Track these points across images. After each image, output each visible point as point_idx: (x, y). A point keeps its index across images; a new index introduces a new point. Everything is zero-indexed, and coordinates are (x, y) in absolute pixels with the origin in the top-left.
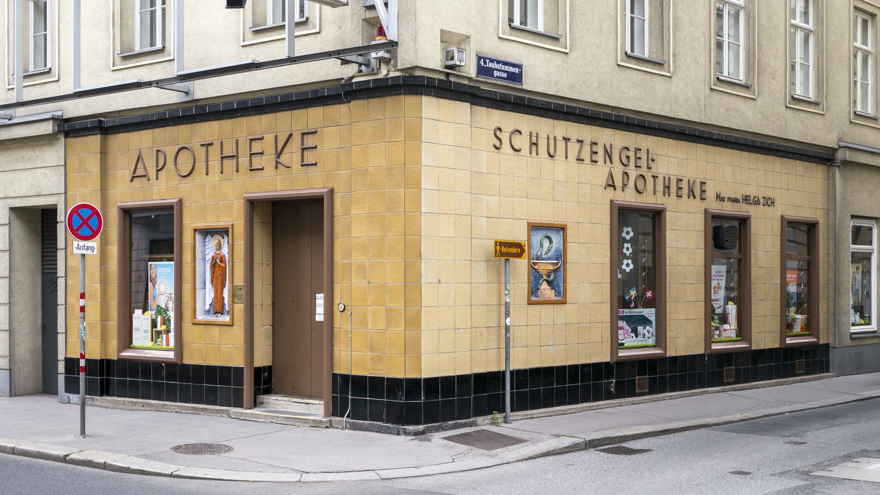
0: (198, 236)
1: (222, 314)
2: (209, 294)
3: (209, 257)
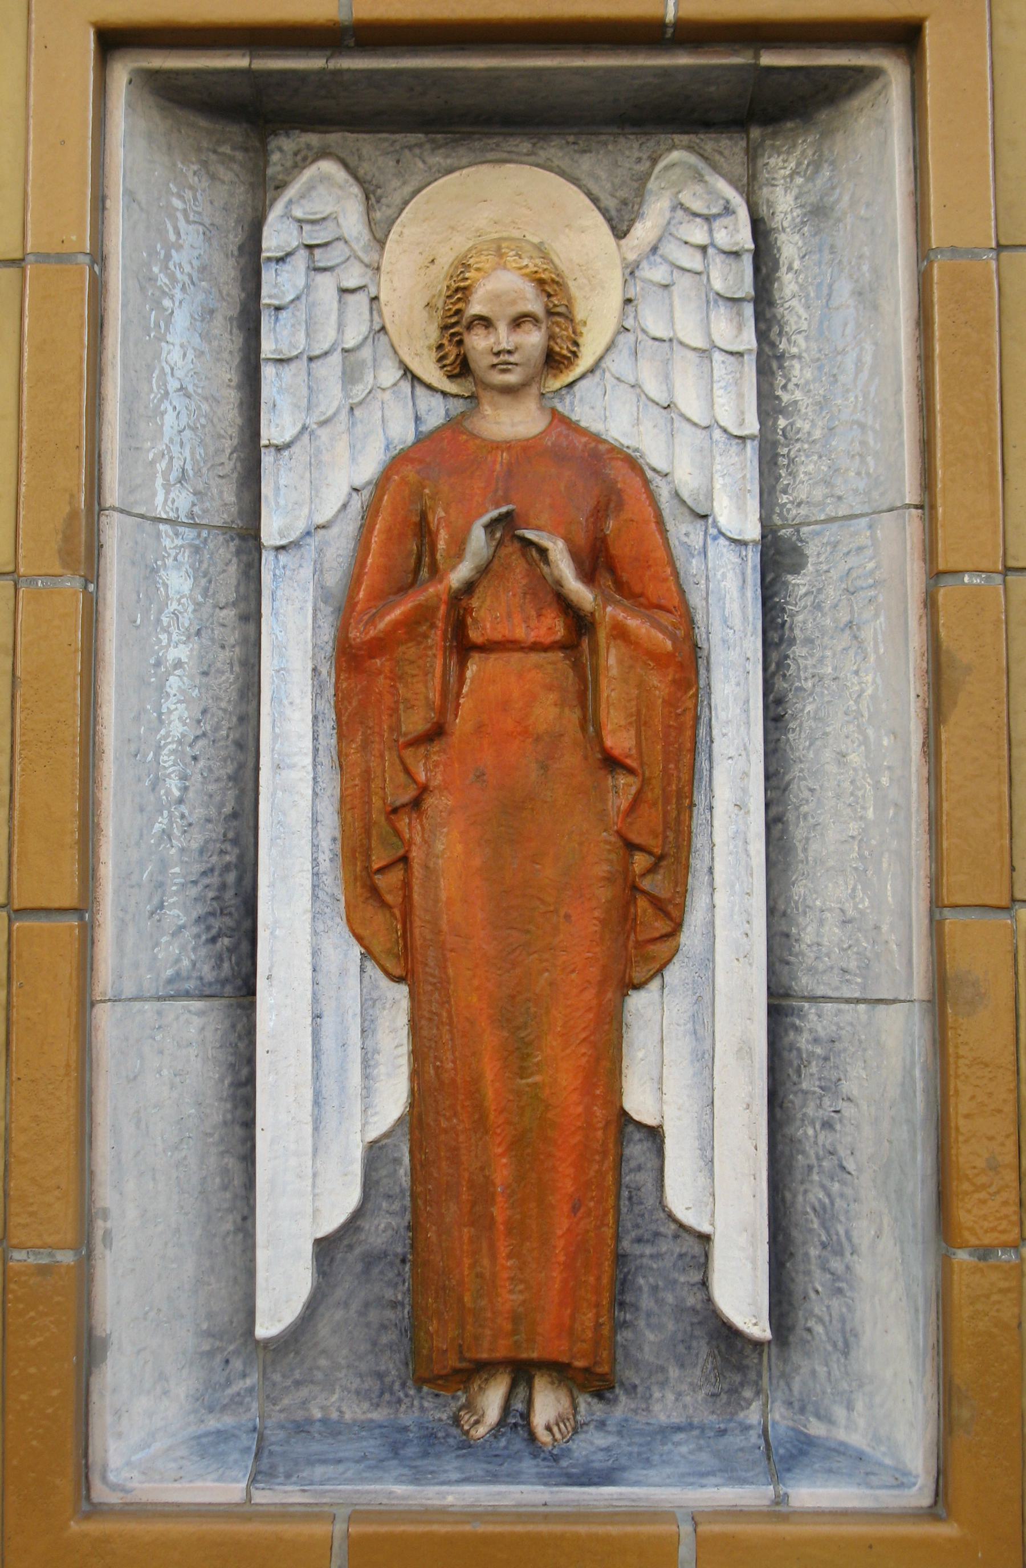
0: (159, 208)
1: (593, 1380)
3: (323, 485)
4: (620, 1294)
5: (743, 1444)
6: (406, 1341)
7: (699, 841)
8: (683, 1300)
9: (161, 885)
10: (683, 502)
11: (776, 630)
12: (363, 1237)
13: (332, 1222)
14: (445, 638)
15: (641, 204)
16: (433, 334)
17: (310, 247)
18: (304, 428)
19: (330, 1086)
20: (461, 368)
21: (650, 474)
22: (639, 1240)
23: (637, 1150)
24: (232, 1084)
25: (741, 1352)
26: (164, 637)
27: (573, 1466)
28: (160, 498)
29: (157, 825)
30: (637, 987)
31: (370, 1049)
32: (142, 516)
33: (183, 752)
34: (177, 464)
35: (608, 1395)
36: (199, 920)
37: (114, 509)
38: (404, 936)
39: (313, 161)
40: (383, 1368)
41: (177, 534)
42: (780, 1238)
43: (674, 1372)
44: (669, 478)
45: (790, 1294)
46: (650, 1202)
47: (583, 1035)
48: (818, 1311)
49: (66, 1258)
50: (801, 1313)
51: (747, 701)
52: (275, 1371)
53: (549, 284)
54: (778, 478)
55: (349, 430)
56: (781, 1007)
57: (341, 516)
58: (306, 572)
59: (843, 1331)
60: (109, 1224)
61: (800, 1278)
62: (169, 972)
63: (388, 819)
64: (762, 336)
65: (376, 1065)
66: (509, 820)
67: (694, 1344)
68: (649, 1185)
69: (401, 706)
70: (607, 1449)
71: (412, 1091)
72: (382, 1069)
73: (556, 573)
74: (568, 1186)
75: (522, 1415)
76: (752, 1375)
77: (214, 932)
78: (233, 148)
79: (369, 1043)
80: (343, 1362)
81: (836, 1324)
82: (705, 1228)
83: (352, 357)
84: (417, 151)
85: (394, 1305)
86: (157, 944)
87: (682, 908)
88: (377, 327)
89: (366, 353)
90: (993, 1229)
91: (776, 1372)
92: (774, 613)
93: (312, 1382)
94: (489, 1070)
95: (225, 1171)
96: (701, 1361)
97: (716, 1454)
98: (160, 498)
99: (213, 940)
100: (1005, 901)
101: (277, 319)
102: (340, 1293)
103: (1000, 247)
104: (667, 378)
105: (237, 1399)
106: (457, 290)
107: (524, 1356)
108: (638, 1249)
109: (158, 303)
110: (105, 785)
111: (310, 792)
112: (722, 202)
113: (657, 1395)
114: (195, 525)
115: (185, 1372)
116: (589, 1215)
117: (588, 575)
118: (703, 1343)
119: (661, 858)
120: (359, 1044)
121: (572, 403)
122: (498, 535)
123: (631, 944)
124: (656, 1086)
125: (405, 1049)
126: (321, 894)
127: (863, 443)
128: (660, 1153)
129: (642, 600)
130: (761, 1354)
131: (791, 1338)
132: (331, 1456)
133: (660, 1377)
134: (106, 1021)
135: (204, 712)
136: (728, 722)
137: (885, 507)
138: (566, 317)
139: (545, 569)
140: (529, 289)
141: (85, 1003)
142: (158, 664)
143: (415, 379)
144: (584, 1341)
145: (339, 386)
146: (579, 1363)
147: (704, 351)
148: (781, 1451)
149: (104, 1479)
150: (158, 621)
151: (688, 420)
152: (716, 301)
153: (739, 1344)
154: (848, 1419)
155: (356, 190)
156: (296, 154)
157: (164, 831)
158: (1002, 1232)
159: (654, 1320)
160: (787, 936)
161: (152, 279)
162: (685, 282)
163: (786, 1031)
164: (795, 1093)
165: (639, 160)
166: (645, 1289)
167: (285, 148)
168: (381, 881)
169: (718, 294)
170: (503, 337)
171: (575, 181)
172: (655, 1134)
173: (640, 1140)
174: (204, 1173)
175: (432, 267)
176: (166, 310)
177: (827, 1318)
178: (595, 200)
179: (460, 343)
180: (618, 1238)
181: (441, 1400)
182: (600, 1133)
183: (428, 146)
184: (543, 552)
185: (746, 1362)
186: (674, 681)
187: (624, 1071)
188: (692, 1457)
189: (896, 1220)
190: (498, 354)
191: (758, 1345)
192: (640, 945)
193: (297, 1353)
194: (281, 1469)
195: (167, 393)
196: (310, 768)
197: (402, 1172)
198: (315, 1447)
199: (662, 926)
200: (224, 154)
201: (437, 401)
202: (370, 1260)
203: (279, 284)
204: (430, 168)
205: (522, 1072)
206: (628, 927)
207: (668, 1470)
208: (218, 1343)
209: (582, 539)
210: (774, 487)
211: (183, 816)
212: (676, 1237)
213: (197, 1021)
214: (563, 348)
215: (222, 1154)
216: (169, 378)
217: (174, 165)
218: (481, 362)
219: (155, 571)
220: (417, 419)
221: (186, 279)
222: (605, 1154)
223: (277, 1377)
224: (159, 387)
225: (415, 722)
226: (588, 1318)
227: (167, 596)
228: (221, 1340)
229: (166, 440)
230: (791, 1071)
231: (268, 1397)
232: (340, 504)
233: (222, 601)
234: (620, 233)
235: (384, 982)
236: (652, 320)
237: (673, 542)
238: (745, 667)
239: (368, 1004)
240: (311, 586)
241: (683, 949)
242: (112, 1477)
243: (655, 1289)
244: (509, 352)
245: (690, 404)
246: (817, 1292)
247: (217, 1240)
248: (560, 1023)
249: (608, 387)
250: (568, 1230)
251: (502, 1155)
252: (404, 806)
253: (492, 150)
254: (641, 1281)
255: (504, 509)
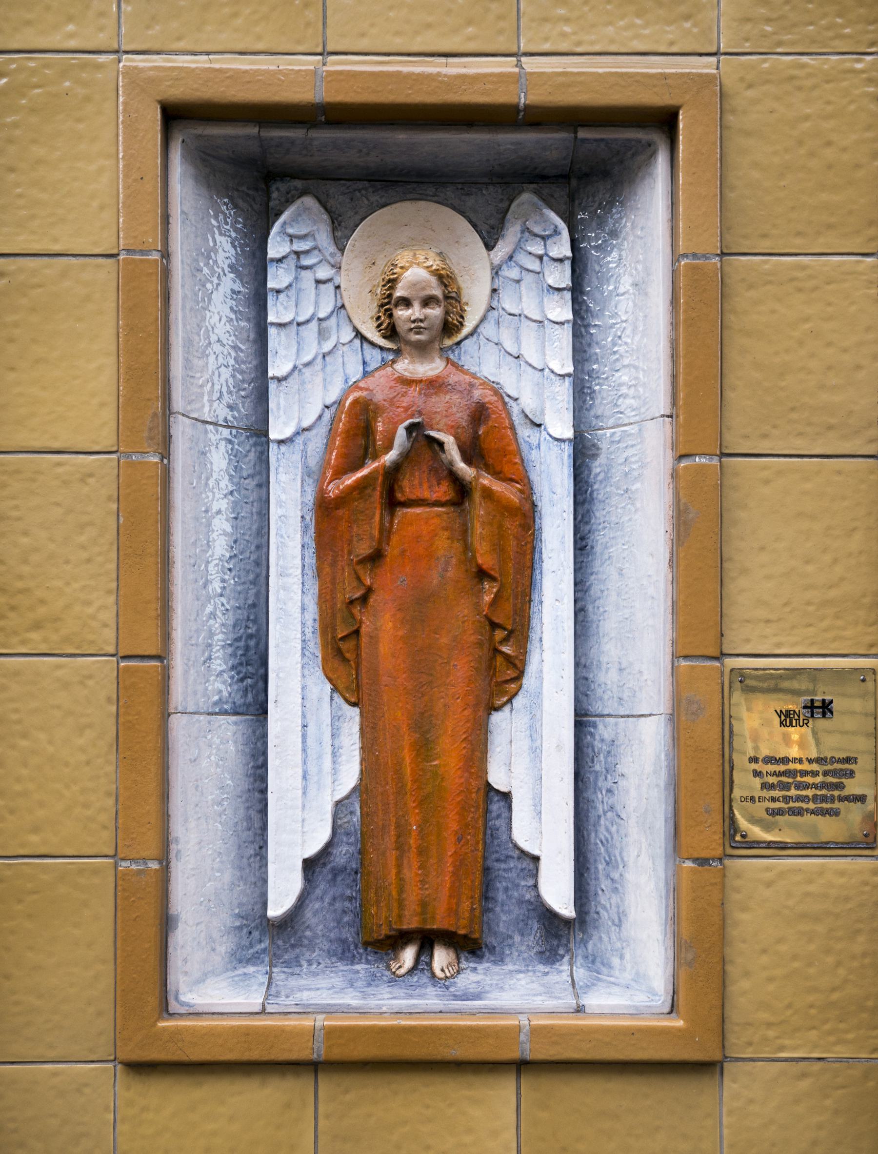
0: (202, 242)
2: (318, 761)
3: (300, 410)
4: (486, 895)
5: (559, 979)
6: (358, 920)
7: (535, 622)
8: (523, 896)
9: (210, 645)
10: (526, 416)
11: (582, 494)
12: (332, 859)
13: (313, 849)
14: (381, 497)
15: (502, 229)
16: (373, 309)
17: (298, 254)
18: (295, 367)
19: (312, 769)
20: (391, 332)
21: (507, 399)
22: (498, 860)
23: (496, 807)
24: (253, 767)
25: (557, 927)
26: (210, 494)
27: (457, 991)
28: (206, 409)
29: (207, 609)
30: (497, 709)
31: (336, 746)
32: (196, 419)
33: (223, 566)
34: (217, 387)
35: (478, 952)
36: (233, 668)
37: (179, 413)
38: (357, 678)
39: (299, 197)
40: (344, 937)
41: (217, 431)
42: (581, 859)
43: (517, 938)
44: (519, 402)
45: (587, 892)
46: (504, 837)
47: (464, 736)
48: (605, 901)
49: (154, 866)
50: (593, 903)
51: (564, 537)
52: (279, 938)
53: (444, 278)
54: (585, 401)
55: (323, 369)
56: (583, 722)
57: (318, 423)
58: (297, 457)
59: (618, 913)
60: (179, 847)
61: (593, 883)
62: (216, 698)
63: (347, 607)
64: (575, 312)
65: (340, 756)
66: (420, 609)
67: (530, 922)
68: (503, 828)
69: (355, 539)
70: (478, 982)
71: (361, 770)
72: (344, 758)
73: (449, 457)
74: (454, 826)
75: (426, 963)
76: (564, 941)
77: (241, 675)
78: (248, 188)
79: (336, 743)
80: (320, 933)
81: (615, 909)
82: (535, 852)
83: (324, 324)
84: (363, 192)
85: (351, 899)
86: (208, 681)
87: (524, 663)
88: (339, 305)
89: (333, 321)
90: (707, 848)
91: (578, 939)
92: (581, 484)
93: (301, 945)
94: (407, 757)
95: (249, 819)
96: (534, 932)
97: (543, 985)
98: (206, 409)
99: (242, 680)
100: (717, 654)
101: (277, 298)
102: (318, 892)
103: (723, 254)
104: (518, 340)
105: (256, 955)
106: (390, 281)
107: (429, 927)
108: (497, 865)
109: (204, 286)
110: (175, 582)
111: (300, 591)
112: (552, 227)
113: (508, 952)
114: (228, 427)
115: (225, 938)
116: (467, 843)
117: (467, 459)
118: (535, 921)
119: (511, 632)
120: (330, 743)
121: (459, 355)
122: (414, 434)
123: (493, 684)
124: (508, 768)
125: (358, 746)
126: (307, 653)
127: (636, 378)
128: (510, 808)
129: (501, 475)
130: (569, 928)
131: (588, 919)
132: (313, 987)
133: (510, 942)
134: (178, 725)
135: (235, 542)
136: (552, 550)
137: (649, 418)
138: (456, 300)
139: (443, 456)
140: (433, 280)
141: (165, 715)
142: (206, 511)
143: (363, 338)
144: (464, 919)
145: (316, 342)
146: (462, 932)
147: (541, 322)
148: (581, 984)
149: (177, 999)
150: (207, 484)
151: (530, 365)
152: (548, 290)
153: (556, 922)
154: (621, 965)
155: (325, 216)
156: (288, 193)
157: (211, 613)
158: (714, 849)
159: (506, 908)
160: (586, 679)
161: (200, 270)
162: (528, 278)
163: (585, 735)
164: (591, 772)
165: (502, 200)
166: (501, 889)
167: (282, 189)
168: (343, 646)
169: (550, 286)
170: (416, 311)
171: (462, 213)
172: (506, 797)
173: (498, 801)
174: (236, 820)
175: (374, 267)
176: (208, 290)
177: (608, 906)
178: (474, 226)
179: (391, 316)
180: (485, 858)
181: (378, 955)
182: (474, 795)
183: (370, 190)
184: (441, 444)
185: (561, 933)
186: (520, 525)
187: (489, 759)
188: (528, 986)
189: (650, 845)
190: (414, 322)
191: (567, 923)
192: (498, 684)
193: (292, 928)
194: (283, 993)
195: (210, 343)
196: (300, 576)
197: (355, 819)
198: (303, 982)
199: (511, 673)
200: (243, 191)
201: (377, 353)
202: (336, 873)
203: (277, 278)
204: (372, 203)
205: (428, 759)
206: (491, 673)
207: (514, 993)
208: (245, 922)
209: (466, 436)
210: (582, 407)
211: (223, 605)
212: (519, 858)
213: (233, 728)
214: (453, 319)
215: (248, 808)
216: (211, 333)
217: (212, 198)
218: (402, 327)
219: (204, 453)
220: (364, 363)
221: (220, 270)
222: (477, 808)
223: (280, 942)
224: (205, 339)
225: (364, 549)
226: (466, 905)
227: (212, 470)
228: (247, 920)
229: (210, 373)
230: (588, 760)
231: (275, 954)
232: (317, 416)
233: (245, 474)
234: (489, 247)
235: (346, 707)
236: (508, 302)
237: (521, 441)
238: (562, 515)
239: (336, 719)
240: (300, 465)
241: (525, 686)
242: (183, 998)
243: (506, 889)
244: (421, 321)
245: (531, 355)
246: (603, 890)
247: (245, 860)
248: (450, 729)
249: (482, 344)
250: (455, 852)
251: (415, 808)
252: (356, 599)
253: (411, 193)
254: (498, 885)
255: (417, 420)
